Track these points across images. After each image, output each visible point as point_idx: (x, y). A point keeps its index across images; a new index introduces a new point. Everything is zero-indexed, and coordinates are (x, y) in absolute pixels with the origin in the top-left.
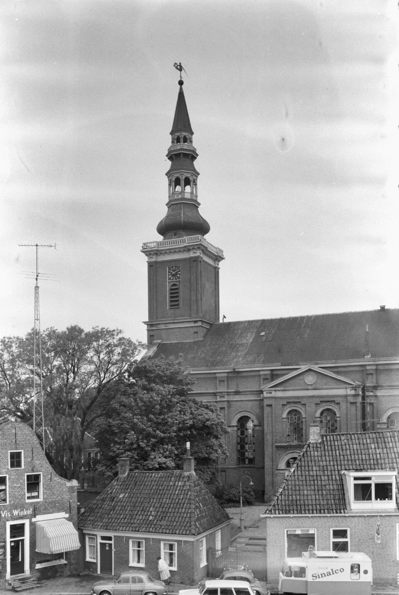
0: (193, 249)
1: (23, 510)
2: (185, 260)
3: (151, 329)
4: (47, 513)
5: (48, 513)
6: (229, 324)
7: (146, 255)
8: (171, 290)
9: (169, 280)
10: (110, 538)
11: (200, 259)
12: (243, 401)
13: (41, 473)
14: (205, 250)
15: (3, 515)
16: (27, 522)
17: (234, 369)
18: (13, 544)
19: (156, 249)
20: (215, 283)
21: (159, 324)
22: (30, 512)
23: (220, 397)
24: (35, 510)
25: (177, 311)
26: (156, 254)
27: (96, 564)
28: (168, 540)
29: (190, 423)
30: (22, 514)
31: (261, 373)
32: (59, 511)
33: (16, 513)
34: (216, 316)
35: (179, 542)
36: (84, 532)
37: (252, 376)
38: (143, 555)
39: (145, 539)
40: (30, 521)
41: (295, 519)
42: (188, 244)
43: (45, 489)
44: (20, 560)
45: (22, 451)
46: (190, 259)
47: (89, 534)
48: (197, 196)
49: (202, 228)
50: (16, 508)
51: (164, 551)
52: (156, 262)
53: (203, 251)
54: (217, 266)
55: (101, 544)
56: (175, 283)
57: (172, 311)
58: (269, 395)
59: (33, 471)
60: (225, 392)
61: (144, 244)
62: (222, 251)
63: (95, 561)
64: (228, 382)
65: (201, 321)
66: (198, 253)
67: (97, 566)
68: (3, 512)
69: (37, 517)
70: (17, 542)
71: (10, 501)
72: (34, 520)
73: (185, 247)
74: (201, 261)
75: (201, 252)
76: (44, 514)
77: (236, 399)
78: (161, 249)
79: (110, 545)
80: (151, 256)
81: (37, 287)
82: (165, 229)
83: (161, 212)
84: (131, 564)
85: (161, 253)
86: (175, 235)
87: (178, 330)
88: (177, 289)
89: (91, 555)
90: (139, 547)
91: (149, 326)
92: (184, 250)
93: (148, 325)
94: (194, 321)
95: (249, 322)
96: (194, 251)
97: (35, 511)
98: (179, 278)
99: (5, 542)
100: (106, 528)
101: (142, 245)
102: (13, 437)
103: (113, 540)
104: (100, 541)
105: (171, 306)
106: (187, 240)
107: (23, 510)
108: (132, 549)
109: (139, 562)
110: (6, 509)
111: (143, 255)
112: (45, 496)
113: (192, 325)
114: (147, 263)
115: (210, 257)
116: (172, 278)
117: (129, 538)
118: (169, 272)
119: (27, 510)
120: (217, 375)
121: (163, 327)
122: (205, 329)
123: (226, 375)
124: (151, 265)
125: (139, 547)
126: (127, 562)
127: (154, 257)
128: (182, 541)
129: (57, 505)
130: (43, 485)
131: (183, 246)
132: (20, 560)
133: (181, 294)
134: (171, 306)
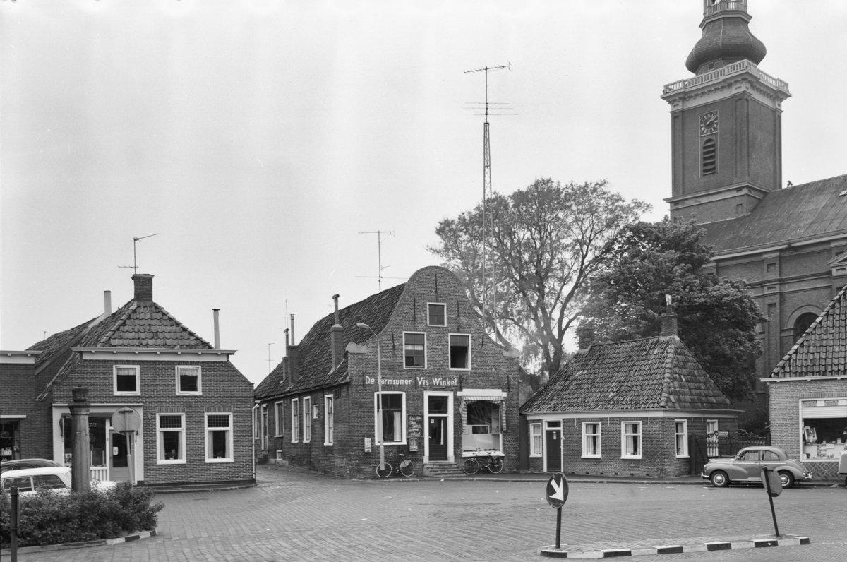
0: (736, 82)
1: (445, 379)
2: (724, 101)
3: (676, 208)
4: (476, 388)
5: (479, 388)
6: (795, 187)
7: (670, 102)
8: (705, 153)
9: (701, 134)
10: (556, 424)
11: (746, 97)
12: (804, 290)
13: (470, 335)
14: (754, 81)
15: (420, 383)
16: (450, 395)
17: (789, 244)
18: (433, 421)
19: (683, 90)
20: (775, 134)
21: (687, 199)
22: (454, 383)
23: (769, 288)
24: (461, 381)
25: (713, 178)
26: (683, 99)
27: (541, 459)
28: (631, 419)
29: (700, 301)
30: (444, 384)
31: (833, 245)
32: (493, 386)
33: (436, 381)
34: (775, 178)
35: (644, 419)
36: (529, 418)
37: (819, 252)
38: (599, 442)
39: (602, 419)
40: (455, 396)
41: (814, 384)
42: (728, 77)
43: (474, 355)
44: (442, 443)
45: (445, 304)
46: (734, 96)
47: (534, 421)
48: (746, 6)
49: (755, 52)
50: (436, 376)
51: (625, 435)
52: (683, 111)
53: (752, 85)
54: (777, 107)
55: (547, 431)
56: (710, 137)
57: (706, 179)
58: (841, 273)
59: (458, 331)
60: (775, 280)
61: (666, 87)
62: (786, 85)
63: (540, 456)
64: (780, 266)
65: (747, 187)
66: (743, 87)
67: (543, 461)
68: (420, 378)
69: (464, 390)
70: (438, 420)
71: (428, 367)
72: (459, 394)
73: (724, 81)
74: (747, 100)
75: (749, 86)
76: (473, 388)
77: (793, 290)
78: (690, 90)
79: (558, 432)
80: (676, 103)
81: (487, 124)
82: (697, 62)
83: (691, 37)
84: (584, 455)
85: (690, 97)
86: (711, 67)
87: (713, 205)
88: (713, 146)
89: (537, 450)
90: (595, 432)
91: (673, 205)
92: (723, 87)
93: (671, 203)
94: (736, 188)
95: (825, 181)
96: (738, 85)
97: (461, 382)
98: (715, 129)
99: (422, 416)
100: (554, 410)
101: (663, 89)
102: (433, 286)
103: (562, 424)
104: (546, 428)
105: (705, 171)
106: (727, 71)
107: (445, 379)
108: (585, 434)
109: (595, 453)
110: (423, 375)
111: (665, 103)
112: (475, 365)
113: (734, 194)
114: (670, 115)
115: (764, 93)
116: (705, 132)
117: (581, 420)
118: (701, 123)
119: (450, 379)
120: (765, 256)
121: (692, 203)
122: (754, 200)
123: (777, 254)
124: (675, 117)
125: (595, 432)
126: (580, 452)
127: (681, 104)
128: (647, 418)
129: (491, 378)
130: (472, 351)
131: (721, 80)
132: (442, 443)
133: (718, 152)
134: (705, 171)
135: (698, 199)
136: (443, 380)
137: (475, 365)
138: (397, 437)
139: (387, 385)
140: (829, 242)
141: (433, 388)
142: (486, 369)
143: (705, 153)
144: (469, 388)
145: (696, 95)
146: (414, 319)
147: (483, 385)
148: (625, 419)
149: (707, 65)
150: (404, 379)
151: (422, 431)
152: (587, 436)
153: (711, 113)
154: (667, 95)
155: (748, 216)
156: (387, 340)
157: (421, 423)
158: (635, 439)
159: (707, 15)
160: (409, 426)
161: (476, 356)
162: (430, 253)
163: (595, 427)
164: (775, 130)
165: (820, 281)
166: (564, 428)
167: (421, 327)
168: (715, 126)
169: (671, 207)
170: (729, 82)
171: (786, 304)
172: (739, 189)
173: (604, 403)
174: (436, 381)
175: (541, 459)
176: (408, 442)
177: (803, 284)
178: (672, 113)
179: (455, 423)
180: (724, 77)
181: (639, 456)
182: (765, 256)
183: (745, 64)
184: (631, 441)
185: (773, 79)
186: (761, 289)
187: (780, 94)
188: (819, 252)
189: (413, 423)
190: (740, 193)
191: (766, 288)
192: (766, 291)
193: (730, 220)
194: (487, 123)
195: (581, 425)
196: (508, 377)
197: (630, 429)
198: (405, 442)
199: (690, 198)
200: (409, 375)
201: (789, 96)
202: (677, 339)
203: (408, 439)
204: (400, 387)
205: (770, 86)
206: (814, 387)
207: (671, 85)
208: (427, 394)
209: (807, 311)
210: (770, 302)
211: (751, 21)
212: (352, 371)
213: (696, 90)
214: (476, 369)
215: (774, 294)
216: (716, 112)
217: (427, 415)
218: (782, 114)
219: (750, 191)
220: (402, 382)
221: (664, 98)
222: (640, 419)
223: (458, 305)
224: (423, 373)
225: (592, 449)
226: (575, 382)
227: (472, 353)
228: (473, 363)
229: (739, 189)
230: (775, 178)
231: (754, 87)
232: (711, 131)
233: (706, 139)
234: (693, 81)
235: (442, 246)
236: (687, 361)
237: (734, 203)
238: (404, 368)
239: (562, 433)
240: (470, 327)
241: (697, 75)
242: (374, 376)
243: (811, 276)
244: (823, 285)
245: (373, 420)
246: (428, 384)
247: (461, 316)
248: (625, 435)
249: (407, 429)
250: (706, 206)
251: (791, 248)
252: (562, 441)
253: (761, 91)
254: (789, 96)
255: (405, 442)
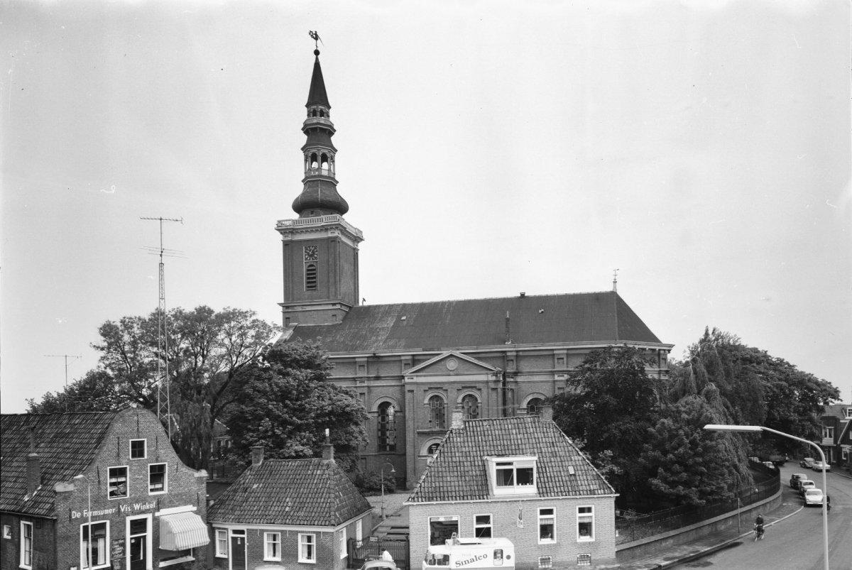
1: (145, 504)
4: (172, 507)
5: (174, 506)
7: (281, 233)
15: (122, 510)
17: (375, 354)
18: (133, 541)
20: (354, 266)
22: (153, 505)
24: (158, 503)
27: (227, 560)
28: (306, 532)
30: (144, 508)
31: (403, 358)
33: (137, 507)
34: (355, 296)
35: (318, 533)
36: (214, 525)
38: (279, 548)
39: (282, 531)
46: (329, 238)
47: (219, 528)
48: (334, 174)
49: (341, 208)
50: (137, 502)
51: (302, 544)
55: (232, 538)
57: (309, 292)
59: (157, 461)
60: (365, 377)
62: (361, 232)
63: (226, 556)
66: (337, 233)
69: (161, 510)
70: (138, 539)
72: (157, 514)
79: (243, 539)
87: (315, 313)
90: (274, 540)
98: (316, 258)
99: (124, 539)
100: (239, 521)
104: (231, 535)
105: (308, 287)
106: (325, 219)
107: (145, 504)
108: (267, 542)
109: (274, 555)
111: (278, 233)
113: (331, 307)
115: (349, 237)
117: (262, 531)
120: (357, 360)
122: (343, 312)
123: (366, 359)
124: (286, 244)
125: (274, 540)
126: (262, 556)
132: (142, 558)
137: (171, 488)
138: (101, 560)
139: (96, 517)
140: (400, 356)
141: (134, 513)
142: (180, 490)
143: (308, 274)
144: (166, 508)
146: (118, 455)
150: (108, 509)
151: (124, 552)
155: (341, 324)
156: (92, 475)
157: (123, 545)
158: (309, 547)
160: (112, 550)
162: (93, 349)
167: (124, 461)
172: (334, 304)
173: (285, 518)
174: (137, 507)
175: (227, 560)
176: (112, 564)
178: (284, 242)
179: (153, 540)
181: (313, 561)
184: (306, 550)
187: (357, 239)
189: (116, 546)
190: (335, 307)
195: (263, 534)
197: (306, 539)
198: (108, 565)
200: (114, 504)
202: (334, 461)
203: (111, 562)
204: (104, 517)
206: (437, 508)
208: (128, 519)
211: (338, 185)
212: (61, 508)
214: (172, 491)
215: (363, 387)
217: (128, 536)
220: (107, 512)
222: (314, 532)
224: (125, 501)
225: (272, 553)
226: (253, 495)
229: (334, 304)
230: (355, 296)
231: (343, 233)
232: (313, 259)
235: (105, 344)
236: (341, 477)
237: (331, 313)
238: (109, 499)
239: (246, 539)
241: (301, 217)
242: (80, 510)
243: (388, 377)
244: (393, 384)
245: (79, 550)
246: (130, 510)
248: (302, 544)
249: (111, 552)
252: (246, 547)
254: (362, 240)
255: (108, 565)
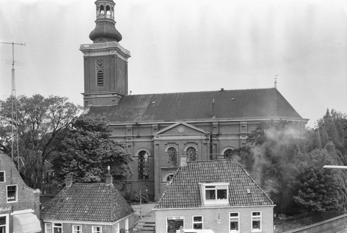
1: (5, 208)
3: (86, 97)
4: (20, 210)
7: (83, 52)
9: (97, 68)
11: (116, 56)
12: (142, 142)
17: (137, 123)
19: (89, 48)
24: (12, 208)
25: (102, 87)
28: (97, 225)
32: (28, 208)
40: (10, 215)
41: (172, 211)
43: (19, 194)
45: (5, 171)
46: (110, 56)
47: (47, 222)
48: (114, 18)
49: (117, 37)
52: (89, 57)
53: (118, 51)
54: (126, 60)
55: (55, 228)
56: (101, 70)
57: (99, 87)
58: (157, 139)
59: (11, 183)
60: (131, 137)
61: (82, 45)
62: (129, 52)
64: (133, 131)
65: (117, 93)
66: (115, 53)
69: (14, 212)
72: (12, 214)
73: (107, 48)
74: (116, 57)
75: (117, 52)
79: (60, 229)
80: (86, 53)
81: (13, 70)
82: (94, 37)
83: (92, 27)
85: (92, 52)
86: (101, 40)
87: (102, 99)
90: (78, 229)
91: (85, 96)
93: (84, 95)
103: (62, 225)
104: (54, 226)
105: (98, 84)
106: (108, 44)
107: (5, 208)
113: (111, 96)
115: (122, 55)
116: (99, 67)
117: (71, 224)
118: (97, 63)
120: (127, 126)
123: (132, 126)
124: (86, 59)
125: (78, 229)
127: (88, 54)
130: (18, 193)
135: (96, 95)
136: (3, 209)
140: (151, 124)
145: (95, 51)
147: (23, 208)
148: (94, 225)
149: (99, 39)
152: (75, 231)
153: (101, 60)
154: (82, 49)
159: (98, 18)
161: (20, 194)
163: (78, 227)
164: (125, 69)
165: (149, 139)
166: (63, 227)
168: (103, 66)
169: (84, 97)
170: (109, 49)
171: (135, 147)
177: (141, 139)
180: (107, 47)
182: (127, 126)
183: (116, 43)
185: (125, 49)
186: (125, 139)
188: (148, 127)
191: (127, 139)
192: (127, 141)
193: (110, 106)
194: (13, 69)
195: (72, 226)
196: (35, 203)
197: (96, 229)
199: (93, 94)
201: (130, 57)
205: (123, 51)
207: (84, 45)
209: (143, 150)
210: (129, 145)
213: (95, 49)
214: (20, 201)
216: (103, 60)
218: (128, 63)
219: (118, 95)
221: (81, 50)
223: (11, 171)
227: (18, 194)
228: (18, 198)
229: (113, 94)
230: (126, 89)
231: (118, 52)
233: (99, 70)
234: (92, 45)
236: (117, 194)
240: (17, 181)
241: (94, 43)
243: (144, 136)
247: (13, 176)
250: (100, 99)
251: (137, 124)
253: (123, 55)
